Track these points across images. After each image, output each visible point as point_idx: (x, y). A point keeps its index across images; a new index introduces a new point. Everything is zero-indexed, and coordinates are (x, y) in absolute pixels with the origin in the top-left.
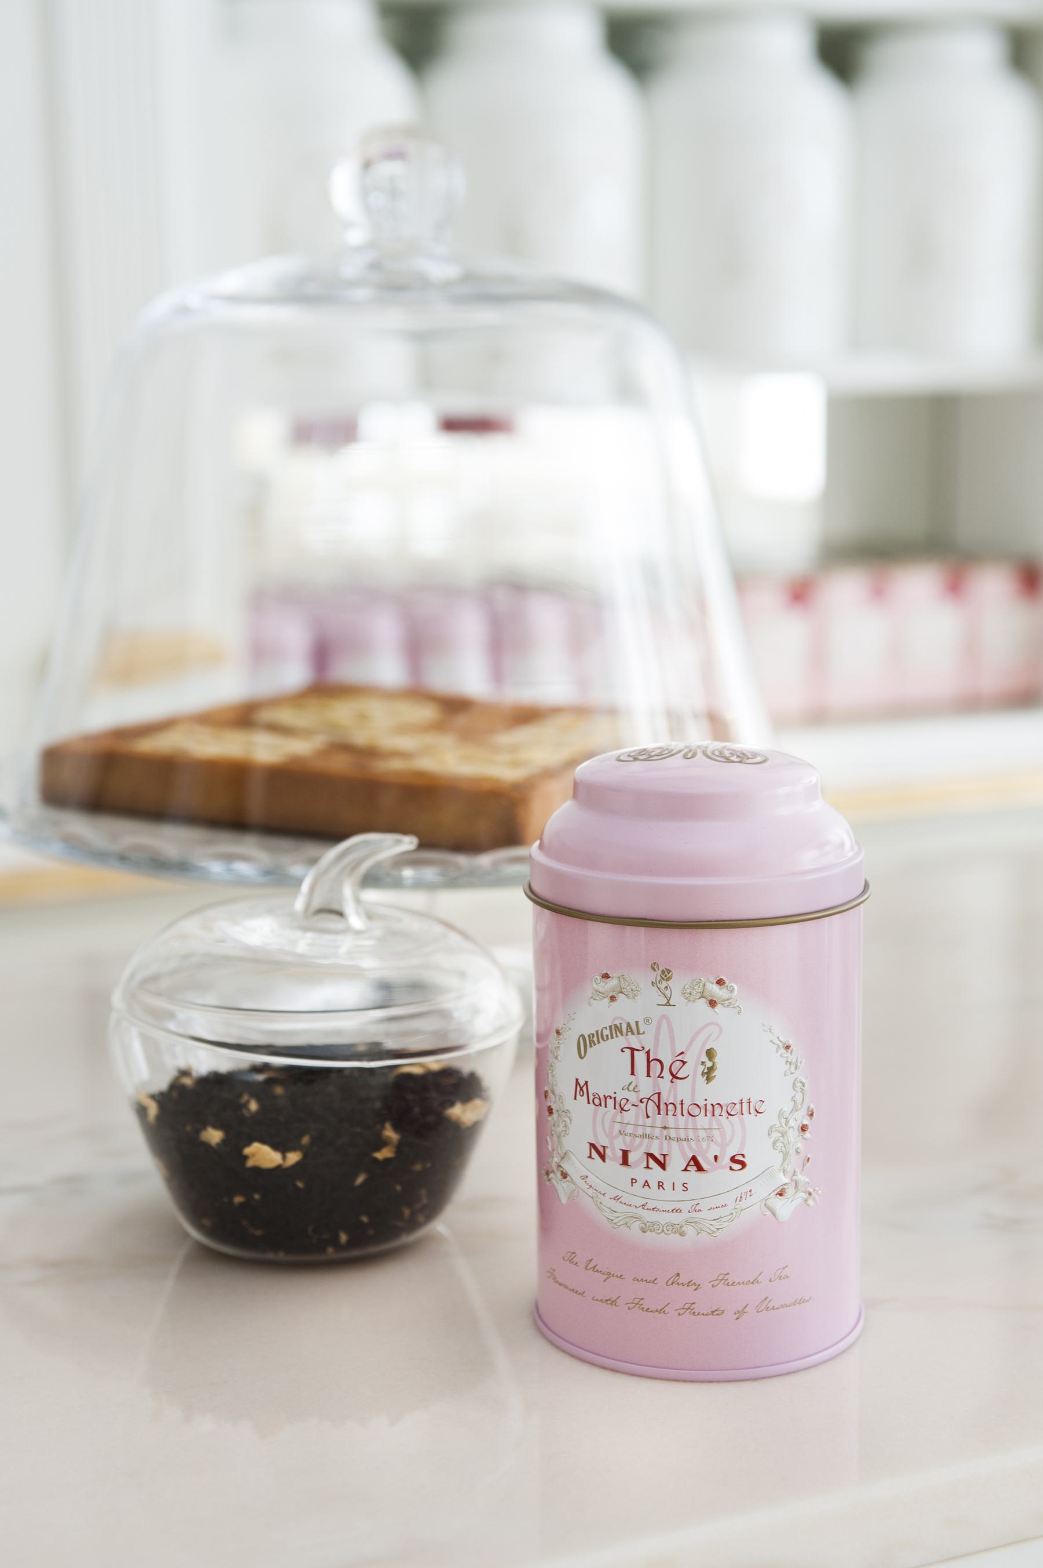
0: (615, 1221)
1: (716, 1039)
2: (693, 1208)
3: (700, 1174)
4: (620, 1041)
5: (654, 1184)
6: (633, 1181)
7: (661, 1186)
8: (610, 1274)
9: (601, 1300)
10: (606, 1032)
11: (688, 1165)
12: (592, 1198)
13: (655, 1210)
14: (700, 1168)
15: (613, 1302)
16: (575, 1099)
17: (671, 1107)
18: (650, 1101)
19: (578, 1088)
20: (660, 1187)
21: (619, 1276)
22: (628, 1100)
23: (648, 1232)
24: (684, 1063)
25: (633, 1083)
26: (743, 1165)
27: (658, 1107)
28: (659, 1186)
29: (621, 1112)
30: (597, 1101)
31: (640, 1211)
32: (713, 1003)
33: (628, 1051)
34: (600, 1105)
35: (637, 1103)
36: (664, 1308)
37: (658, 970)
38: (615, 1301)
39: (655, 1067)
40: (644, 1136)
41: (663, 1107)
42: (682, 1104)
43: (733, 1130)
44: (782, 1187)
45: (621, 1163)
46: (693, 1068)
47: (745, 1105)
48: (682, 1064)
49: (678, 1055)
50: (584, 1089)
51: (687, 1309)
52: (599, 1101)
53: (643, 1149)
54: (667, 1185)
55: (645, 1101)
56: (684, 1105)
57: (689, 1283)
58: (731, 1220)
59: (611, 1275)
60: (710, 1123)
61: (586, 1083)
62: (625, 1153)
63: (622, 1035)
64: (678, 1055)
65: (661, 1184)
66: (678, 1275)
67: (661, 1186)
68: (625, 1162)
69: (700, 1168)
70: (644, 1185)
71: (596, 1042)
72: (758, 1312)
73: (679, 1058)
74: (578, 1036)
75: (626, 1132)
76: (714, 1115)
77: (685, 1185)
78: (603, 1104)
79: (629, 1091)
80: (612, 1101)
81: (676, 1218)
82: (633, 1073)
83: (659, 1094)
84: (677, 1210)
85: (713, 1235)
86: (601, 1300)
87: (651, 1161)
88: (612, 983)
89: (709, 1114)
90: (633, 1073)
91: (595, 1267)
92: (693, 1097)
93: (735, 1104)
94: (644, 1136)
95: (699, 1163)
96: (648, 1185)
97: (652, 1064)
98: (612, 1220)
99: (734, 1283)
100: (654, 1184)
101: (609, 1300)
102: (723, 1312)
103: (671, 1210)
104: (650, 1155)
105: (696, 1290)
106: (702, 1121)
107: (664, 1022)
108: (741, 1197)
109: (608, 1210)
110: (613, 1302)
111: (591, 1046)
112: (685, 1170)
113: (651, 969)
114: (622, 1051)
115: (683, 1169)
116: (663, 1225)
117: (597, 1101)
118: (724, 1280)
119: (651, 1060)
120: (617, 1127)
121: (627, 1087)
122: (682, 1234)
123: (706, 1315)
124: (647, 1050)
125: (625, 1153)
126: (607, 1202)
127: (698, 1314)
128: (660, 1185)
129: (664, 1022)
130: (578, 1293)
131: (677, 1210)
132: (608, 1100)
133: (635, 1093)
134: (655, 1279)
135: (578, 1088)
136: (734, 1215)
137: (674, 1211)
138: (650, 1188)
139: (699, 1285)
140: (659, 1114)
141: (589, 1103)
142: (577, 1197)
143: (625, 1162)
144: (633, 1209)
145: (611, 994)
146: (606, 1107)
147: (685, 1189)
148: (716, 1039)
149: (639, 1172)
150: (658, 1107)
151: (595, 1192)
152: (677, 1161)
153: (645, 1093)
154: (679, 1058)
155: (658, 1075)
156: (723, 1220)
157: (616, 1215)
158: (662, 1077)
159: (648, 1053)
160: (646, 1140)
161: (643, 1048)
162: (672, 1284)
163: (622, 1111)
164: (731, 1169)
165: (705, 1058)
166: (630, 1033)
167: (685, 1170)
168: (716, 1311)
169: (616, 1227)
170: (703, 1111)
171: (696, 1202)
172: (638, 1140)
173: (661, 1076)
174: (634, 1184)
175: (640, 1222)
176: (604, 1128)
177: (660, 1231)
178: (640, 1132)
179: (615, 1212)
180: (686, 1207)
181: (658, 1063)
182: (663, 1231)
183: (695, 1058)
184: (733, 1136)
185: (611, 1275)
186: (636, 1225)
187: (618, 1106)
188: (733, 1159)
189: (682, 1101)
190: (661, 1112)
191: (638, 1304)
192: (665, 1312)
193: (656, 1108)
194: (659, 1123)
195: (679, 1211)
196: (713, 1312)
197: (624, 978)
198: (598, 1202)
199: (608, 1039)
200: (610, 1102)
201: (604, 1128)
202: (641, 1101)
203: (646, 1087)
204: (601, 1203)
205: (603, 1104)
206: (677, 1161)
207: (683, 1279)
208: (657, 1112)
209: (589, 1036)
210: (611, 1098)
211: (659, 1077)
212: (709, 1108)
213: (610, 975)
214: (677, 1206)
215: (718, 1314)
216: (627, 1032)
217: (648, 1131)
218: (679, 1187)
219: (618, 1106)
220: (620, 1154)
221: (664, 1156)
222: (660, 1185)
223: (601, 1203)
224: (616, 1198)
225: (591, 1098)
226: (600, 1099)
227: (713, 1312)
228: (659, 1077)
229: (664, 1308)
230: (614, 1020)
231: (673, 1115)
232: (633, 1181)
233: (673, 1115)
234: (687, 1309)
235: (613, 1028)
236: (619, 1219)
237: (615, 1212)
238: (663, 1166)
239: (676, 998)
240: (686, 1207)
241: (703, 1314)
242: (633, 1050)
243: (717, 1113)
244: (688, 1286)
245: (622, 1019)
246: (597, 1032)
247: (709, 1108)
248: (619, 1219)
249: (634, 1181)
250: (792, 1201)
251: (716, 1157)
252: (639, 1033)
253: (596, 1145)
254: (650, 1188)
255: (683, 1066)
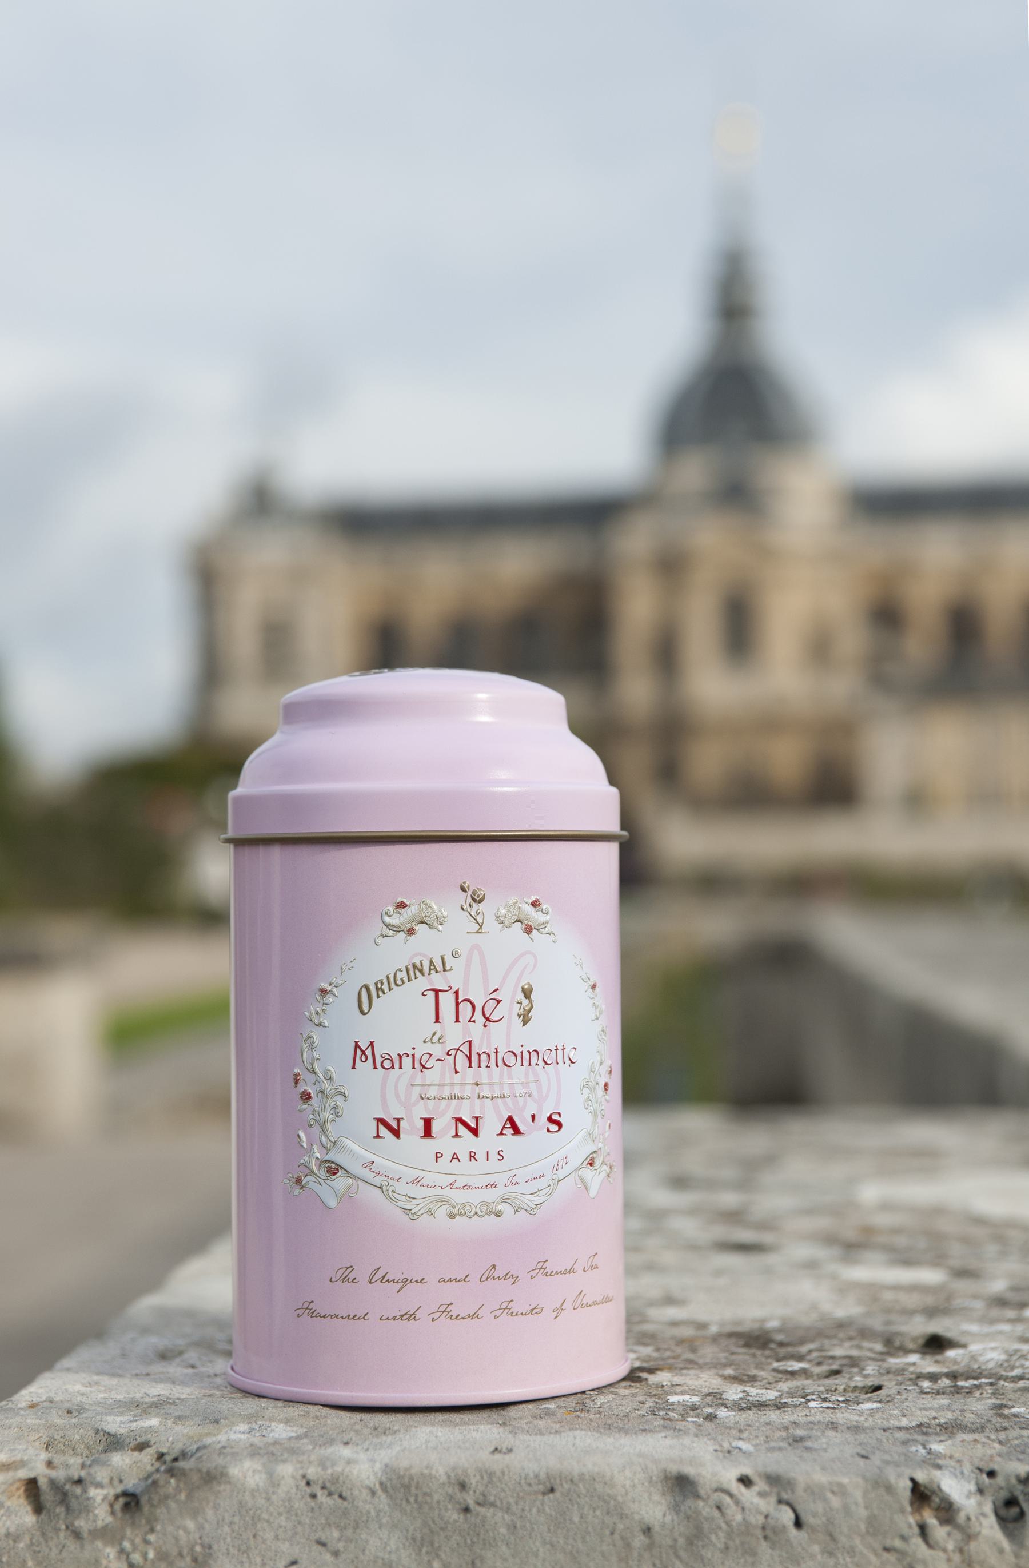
0: (413, 1211)
1: (533, 970)
2: (509, 1181)
3: (517, 1137)
4: (422, 983)
5: (464, 1157)
6: (438, 1156)
7: (474, 1157)
8: (408, 1280)
9: (394, 1318)
10: (401, 975)
11: (504, 1127)
12: (380, 1188)
13: (466, 1187)
14: (517, 1131)
15: (411, 1315)
16: (354, 1068)
17: (484, 1057)
18: (459, 1051)
19: (359, 1053)
20: (472, 1158)
21: (419, 1281)
22: (431, 1055)
23: (458, 1217)
24: (499, 1002)
25: (437, 1034)
26: (559, 1125)
27: (470, 1059)
28: (471, 1156)
29: (422, 1071)
30: (387, 1064)
31: (447, 1192)
32: (528, 930)
33: (432, 994)
34: (393, 1067)
35: (444, 1056)
36: (477, 1312)
37: (469, 890)
38: (414, 1314)
39: (465, 1009)
40: (452, 1097)
41: (474, 1058)
42: (497, 1052)
43: (549, 1080)
44: (591, 1156)
45: (423, 1135)
46: (508, 1010)
47: (560, 1052)
48: (429, 1056)
49: (492, 993)
50: (369, 1052)
51: (505, 1309)
52: (394, 1062)
53: (452, 1113)
54: (481, 1156)
55: (453, 1052)
56: (498, 1053)
57: (506, 1275)
58: (550, 1192)
59: (409, 1281)
60: (527, 1075)
61: (372, 1044)
62: (428, 1123)
63: (423, 974)
64: (492, 993)
65: (473, 1154)
66: (494, 1266)
67: (474, 1157)
68: (428, 1133)
69: (517, 1131)
70: (453, 1158)
71: (386, 989)
72: (574, 1309)
73: (493, 996)
74: (361, 986)
75: (428, 1095)
76: (530, 1065)
77: (500, 1153)
78: (397, 1065)
79: (432, 1043)
80: (410, 1059)
81: (490, 1195)
82: (437, 1021)
83: (470, 1042)
84: (492, 1185)
85: (531, 1212)
86: (394, 1318)
87: (460, 1126)
88: (407, 913)
89: (526, 1063)
90: (437, 1021)
91: (384, 1277)
92: (508, 1045)
93: (551, 1051)
94: (452, 1097)
95: (516, 1124)
96: (457, 1158)
97: (461, 1006)
98: (410, 1210)
99: (552, 1272)
100: (464, 1157)
101: (405, 1314)
102: (542, 1310)
103: (484, 1187)
104: (459, 1120)
105: (514, 1283)
106: (519, 1072)
107: (476, 952)
108: (558, 1165)
109: (403, 1198)
110: (411, 1315)
111: (378, 997)
112: (501, 1134)
113: (461, 891)
114: (423, 995)
115: (499, 1133)
116: (476, 1205)
117: (387, 1064)
118: (542, 1269)
119: (460, 1001)
120: (416, 1091)
121: (429, 1038)
122: (498, 1215)
123: (525, 1314)
124: (454, 989)
125: (428, 1123)
126: (401, 1188)
127: (517, 1314)
128: (472, 1156)
129: (476, 952)
130: (351, 1317)
131: (492, 1185)
132: (404, 1058)
133: (440, 1045)
134: (366, 1315)
135: (359, 1053)
136: (552, 1187)
137: (489, 1186)
138: (459, 1161)
139: (517, 1277)
140: (470, 1067)
141: (375, 1068)
142: (357, 1192)
143: (428, 1133)
144: (438, 1191)
145: (408, 926)
146: (401, 1068)
147: (501, 1158)
148: (533, 970)
149: (444, 1140)
150: (470, 1059)
151: (386, 1179)
152: (491, 1125)
153: (452, 1043)
154: (493, 996)
155: (469, 1019)
156: (541, 1193)
157: (415, 1202)
158: (474, 1022)
159: (457, 993)
160: (454, 1102)
161: (451, 987)
162: (487, 1280)
163: (424, 1070)
164: (548, 1130)
165: (520, 996)
166: (433, 972)
167: (501, 1134)
168: (535, 1308)
169: (416, 1217)
170: (519, 1059)
171: (512, 1173)
172: (444, 1102)
173: (472, 1020)
174: (438, 1159)
175: (448, 1206)
176: (398, 1097)
177: (472, 1214)
178: (446, 1093)
179: (414, 1198)
180: (501, 1179)
181: (468, 1003)
182: (476, 1213)
183: (510, 995)
184: (548, 1091)
185: (409, 1281)
186: (442, 1212)
187: (417, 1065)
188: (550, 1120)
189: (496, 1049)
190: (473, 1065)
191: (446, 1311)
192: (479, 1316)
193: (467, 1060)
194: (470, 1080)
195: (494, 1186)
196: (532, 1310)
197: (426, 905)
198: (390, 1192)
199: (403, 982)
200: (407, 1062)
201: (398, 1097)
202: (448, 1054)
203: (454, 1035)
204: (393, 1192)
205: (397, 1065)
206: (491, 1125)
207: (500, 1272)
208: (468, 1065)
209: (376, 984)
210: (408, 1056)
211: (470, 1021)
212: (526, 1055)
213: (408, 903)
214: (491, 1179)
215: (536, 1313)
216: (430, 970)
217: (457, 1091)
218: (494, 1156)
219: (417, 1065)
220: (421, 1124)
221: (477, 1118)
222: (472, 1156)
223: (393, 1192)
224: (416, 1181)
225: (379, 1060)
226: (392, 1060)
227: (532, 1310)
228: (470, 1021)
229: (477, 1312)
230: (412, 957)
231: (487, 1067)
232: (438, 1156)
233: (487, 1067)
234: (505, 1309)
235: (411, 968)
236: (419, 1207)
237: (414, 1198)
238: (475, 1132)
239: (490, 924)
240: (501, 1179)
241: (522, 1314)
242: (437, 992)
243: (533, 1062)
244: (505, 1279)
245: (425, 956)
246: (388, 978)
247: (526, 1055)
248: (419, 1207)
249: (439, 1155)
250: (599, 1174)
251: (533, 1117)
252: (445, 970)
253: (386, 1119)
254: (459, 1161)
255: (497, 1005)
